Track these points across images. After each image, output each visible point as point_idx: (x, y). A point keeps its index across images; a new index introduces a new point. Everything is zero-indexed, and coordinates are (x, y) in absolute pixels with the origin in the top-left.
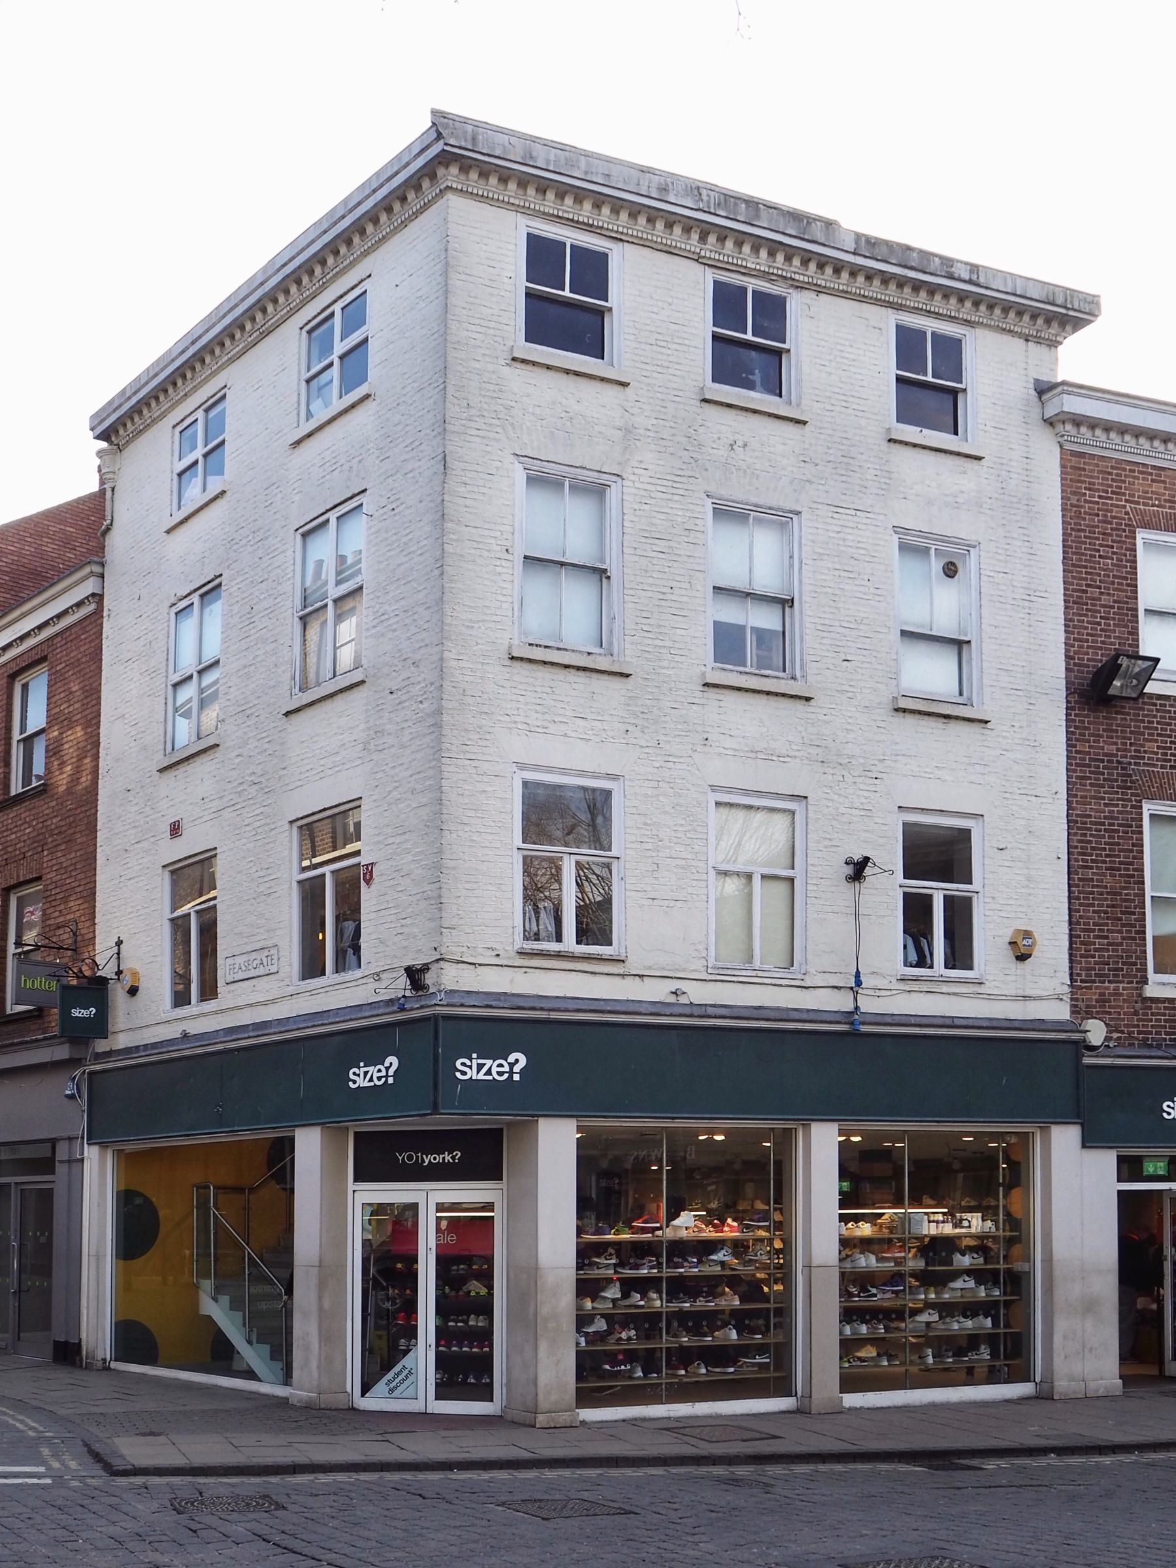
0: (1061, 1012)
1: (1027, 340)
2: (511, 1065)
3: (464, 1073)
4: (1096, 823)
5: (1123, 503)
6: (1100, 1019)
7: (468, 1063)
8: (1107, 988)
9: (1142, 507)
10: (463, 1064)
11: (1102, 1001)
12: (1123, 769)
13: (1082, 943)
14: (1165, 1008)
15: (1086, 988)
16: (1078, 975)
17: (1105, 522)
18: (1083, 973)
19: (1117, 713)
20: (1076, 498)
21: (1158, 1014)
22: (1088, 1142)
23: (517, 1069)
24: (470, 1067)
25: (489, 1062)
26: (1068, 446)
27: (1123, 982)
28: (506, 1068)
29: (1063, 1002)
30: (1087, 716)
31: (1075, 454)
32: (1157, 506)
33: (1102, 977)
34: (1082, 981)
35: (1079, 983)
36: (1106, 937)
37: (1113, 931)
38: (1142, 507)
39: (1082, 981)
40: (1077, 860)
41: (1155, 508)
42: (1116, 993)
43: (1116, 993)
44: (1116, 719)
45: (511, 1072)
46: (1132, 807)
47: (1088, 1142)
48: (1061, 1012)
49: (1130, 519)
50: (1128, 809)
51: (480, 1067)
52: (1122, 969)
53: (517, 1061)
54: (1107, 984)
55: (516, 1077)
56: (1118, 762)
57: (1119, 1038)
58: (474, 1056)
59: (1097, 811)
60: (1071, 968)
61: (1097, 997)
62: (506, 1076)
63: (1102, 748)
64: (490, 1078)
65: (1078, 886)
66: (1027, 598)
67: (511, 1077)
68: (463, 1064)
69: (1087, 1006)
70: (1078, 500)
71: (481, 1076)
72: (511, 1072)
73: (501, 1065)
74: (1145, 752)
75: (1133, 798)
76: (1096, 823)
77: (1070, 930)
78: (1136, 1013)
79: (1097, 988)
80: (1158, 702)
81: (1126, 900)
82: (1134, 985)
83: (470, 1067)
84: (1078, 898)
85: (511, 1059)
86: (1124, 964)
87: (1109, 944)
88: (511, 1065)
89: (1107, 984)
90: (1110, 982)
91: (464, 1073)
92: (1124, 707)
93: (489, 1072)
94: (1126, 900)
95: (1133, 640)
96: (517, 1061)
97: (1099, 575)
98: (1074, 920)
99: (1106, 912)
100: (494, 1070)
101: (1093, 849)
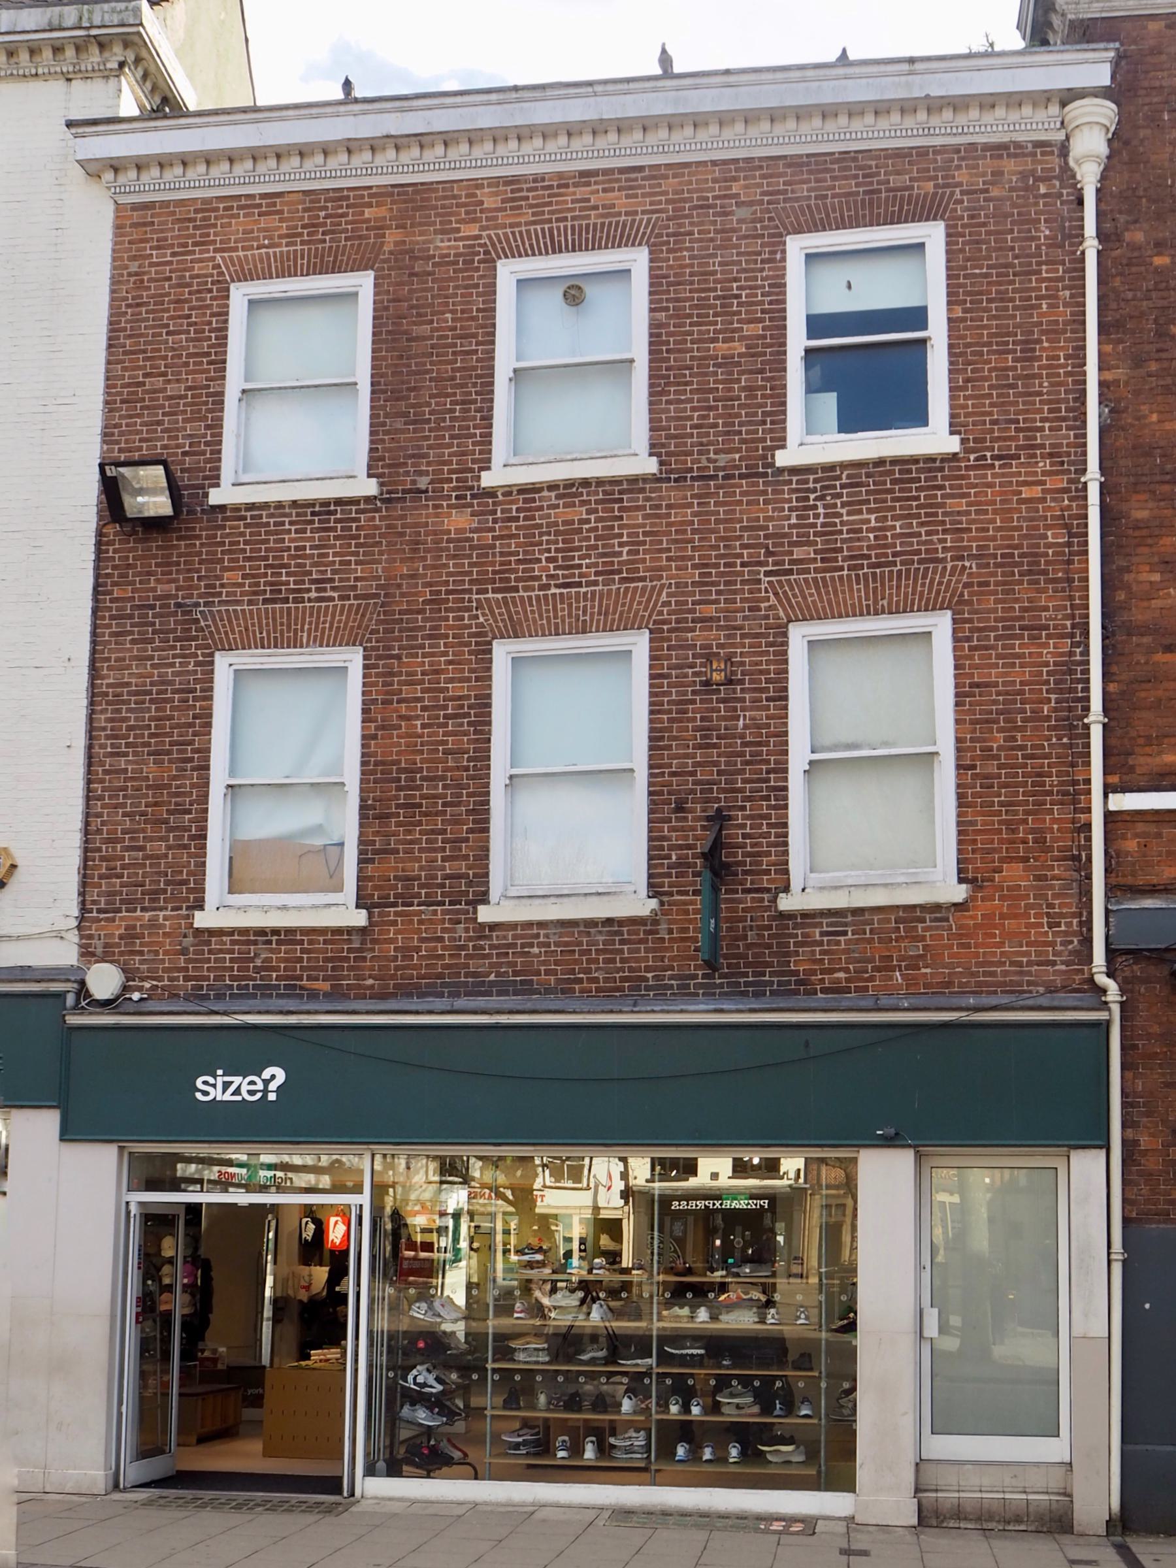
0: (66, 954)
1: (69, 80)
2: (266, 1083)
3: (206, 1093)
4: (137, 693)
5: (211, 254)
6: (111, 962)
7: (211, 1080)
8: (138, 919)
9: (241, 253)
10: (205, 1083)
11: (130, 935)
12: (184, 613)
13: (102, 859)
14: (233, 942)
15: (107, 919)
16: (94, 902)
17: (179, 286)
18: (103, 899)
19: (179, 539)
20: (137, 263)
21: (221, 951)
22: (68, 1133)
23: (273, 1086)
24: (214, 1086)
25: (237, 1080)
26: (122, 200)
27: (166, 909)
28: (260, 1086)
29: (64, 943)
30: (134, 549)
31: (135, 207)
32: (267, 247)
33: (131, 904)
34: (99, 911)
35: (95, 914)
36: (141, 849)
37: (151, 839)
38: (241, 253)
39: (99, 911)
40: (103, 746)
41: (263, 251)
42: (153, 925)
43: (153, 925)
44: (178, 547)
45: (265, 1091)
46: (197, 664)
47: (68, 1133)
48: (66, 954)
49: (221, 274)
50: (191, 667)
51: (226, 1085)
52: (165, 891)
53: (273, 1077)
54: (138, 913)
55: (272, 1097)
56: (178, 605)
57: (154, 988)
58: (220, 1072)
59: (140, 676)
60: (82, 894)
61: (122, 931)
62: (259, 1095)
63: (154, 590)
64: (239, 1098)
65: (102, 781)
66: (42, 409)
67: (265, 1096)
68: (205, 1083)
69: (106, 945)
70: (139, 267)
71: (228, 1097)
72: (265, 1091)
73: (252, 1083)
74: (222, 586)
75: (199, 652)
76: (137, 693)
77: (86, 842)
78: (184, 952)
79: (121, 919)
80: (249, 514)
81: (177, 795)
82: (184, 912)
83: (214, 1086)
84: (101, 798)
85: (266, 1074)
86: (167, 883)
87: (146, 857)
88: (266, 1083)
89: (138, 913)
90: (143, 909)
91: (206, 1093)
92: (194, 529)
93: (237, 1092)
94: (177, 795)
95: (378, 416)
96: (273, 1077)
97: (165, 358)
98: (93, 828)
99: (143, 814)
100: (245, 1088)
101: (130, 728)
